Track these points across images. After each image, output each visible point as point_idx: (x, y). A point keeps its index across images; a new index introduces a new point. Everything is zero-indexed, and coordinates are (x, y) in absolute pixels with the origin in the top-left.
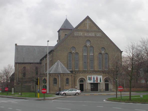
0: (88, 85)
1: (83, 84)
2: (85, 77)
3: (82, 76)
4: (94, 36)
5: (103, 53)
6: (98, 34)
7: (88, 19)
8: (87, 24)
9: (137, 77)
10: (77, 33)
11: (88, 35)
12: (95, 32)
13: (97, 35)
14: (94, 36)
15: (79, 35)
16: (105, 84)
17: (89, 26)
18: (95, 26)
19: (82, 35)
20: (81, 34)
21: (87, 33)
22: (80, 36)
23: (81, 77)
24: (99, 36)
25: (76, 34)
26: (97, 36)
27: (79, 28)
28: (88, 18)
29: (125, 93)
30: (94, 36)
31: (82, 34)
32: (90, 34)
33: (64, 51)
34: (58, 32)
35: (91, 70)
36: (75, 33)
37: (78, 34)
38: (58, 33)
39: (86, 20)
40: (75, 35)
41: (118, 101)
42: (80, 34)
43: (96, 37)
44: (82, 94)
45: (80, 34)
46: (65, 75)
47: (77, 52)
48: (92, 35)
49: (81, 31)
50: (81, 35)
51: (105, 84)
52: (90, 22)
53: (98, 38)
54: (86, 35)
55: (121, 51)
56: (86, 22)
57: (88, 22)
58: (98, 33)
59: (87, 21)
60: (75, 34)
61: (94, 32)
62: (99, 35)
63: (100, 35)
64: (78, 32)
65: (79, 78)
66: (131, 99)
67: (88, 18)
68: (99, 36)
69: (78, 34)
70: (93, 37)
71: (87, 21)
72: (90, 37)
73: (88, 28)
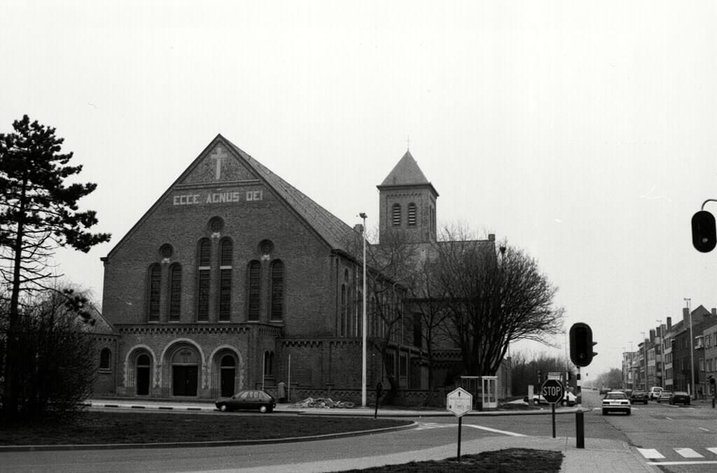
0: (158, 373)
1: (222, 366)
2: (151, 348)
3: (141, 343)
4: (237, 200)
5: (266, 260)
7: (219, 144)
8: (215, 161)
10: (182, 197)
11: (217, 201)
12: (242, 189)
13: (247, 196)
14: (237, 200)
15: (188, 203)
16: (222, 370)
17: (222, 168)
18: (244, 168)
19: (197, 203)
20: (195, 199)
21: (214, 195)
23: (136, 347)
24: (253, 202)
25: (178, 200)
26: (248, 199)
27: (188, 181)
28: (219, 141)
29: (145, 406)
30: (236, 203)
31: (198, 199)
32: (224, 198)
33: (136, 260)
35: (200, 322)
36: (175, 197)
37: (184, 200)
39: (213, 151)
40: (175, 204)
41: (356, 417)
42: (191, 199)
43: (243, 203)
45: (257, 197)
46: (105, 339)
48: (231, 200)
49: (196, 189)
50: (195, 202)
51: (234, 365)
52: (225, 155)
53: (249, 210)
54: (209, 200)
55: (102, 262)
56: (213, 156)
57: (220, 155)
58: (250, 190)
59: (216, 153)
60: (175, 200)
61: (237, 188)
62: (255, 196)
63: (258, 196)
65: (132, 349)
66: (551, 408)
67: (219, 141)
68: (255, 199)
70: (233, 204)
71: (216, 153)
72: (225, 206)
73: (218, 177)
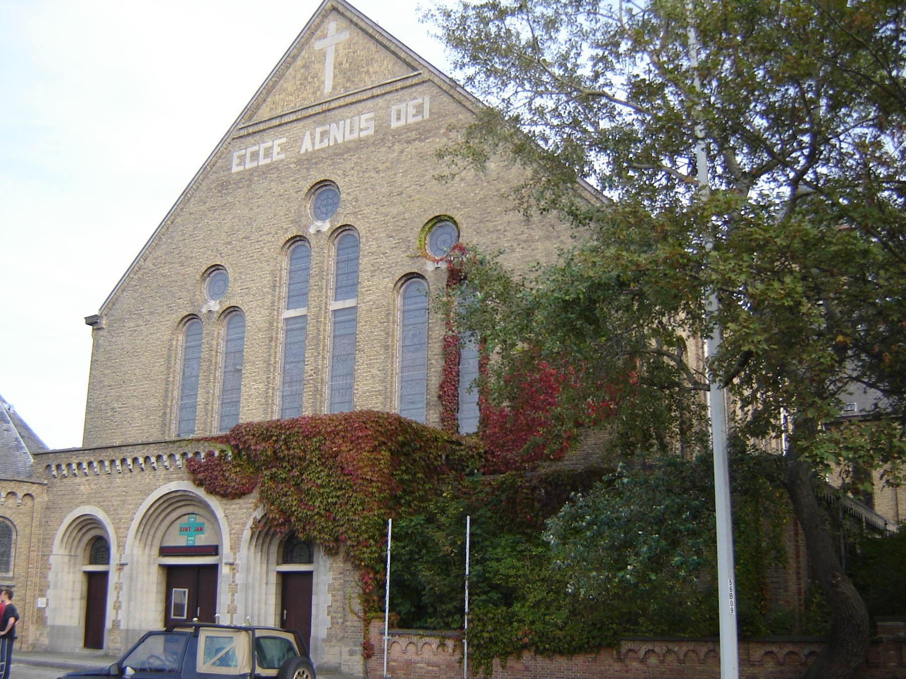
1: (310, 574)
6: (402, 106)
9: (837, 408)
19: (282, 156)
21: (319, 130)
22: (265, 171)
27: (264, 113)
30: (366, 140)
31: (283, 148)
34: (92, 321)
38: (90, 341)
39: (319, 33)
42: (268, 152)
44: (48, 597)
47: (233, 303)
48: (355, 136)
49: (278, 123)
52: (345, 36)
54: (307, 146)
56: (318, 45)
64: (257, 137)
69: (255, 156)
73: (328, 88)
